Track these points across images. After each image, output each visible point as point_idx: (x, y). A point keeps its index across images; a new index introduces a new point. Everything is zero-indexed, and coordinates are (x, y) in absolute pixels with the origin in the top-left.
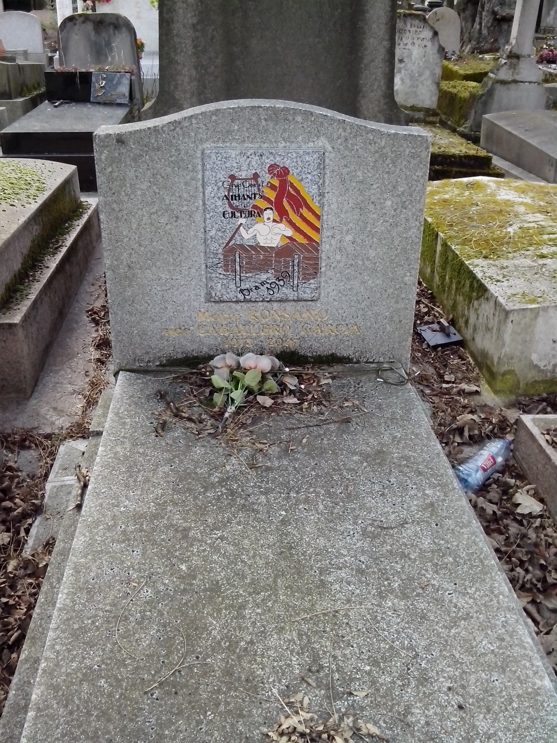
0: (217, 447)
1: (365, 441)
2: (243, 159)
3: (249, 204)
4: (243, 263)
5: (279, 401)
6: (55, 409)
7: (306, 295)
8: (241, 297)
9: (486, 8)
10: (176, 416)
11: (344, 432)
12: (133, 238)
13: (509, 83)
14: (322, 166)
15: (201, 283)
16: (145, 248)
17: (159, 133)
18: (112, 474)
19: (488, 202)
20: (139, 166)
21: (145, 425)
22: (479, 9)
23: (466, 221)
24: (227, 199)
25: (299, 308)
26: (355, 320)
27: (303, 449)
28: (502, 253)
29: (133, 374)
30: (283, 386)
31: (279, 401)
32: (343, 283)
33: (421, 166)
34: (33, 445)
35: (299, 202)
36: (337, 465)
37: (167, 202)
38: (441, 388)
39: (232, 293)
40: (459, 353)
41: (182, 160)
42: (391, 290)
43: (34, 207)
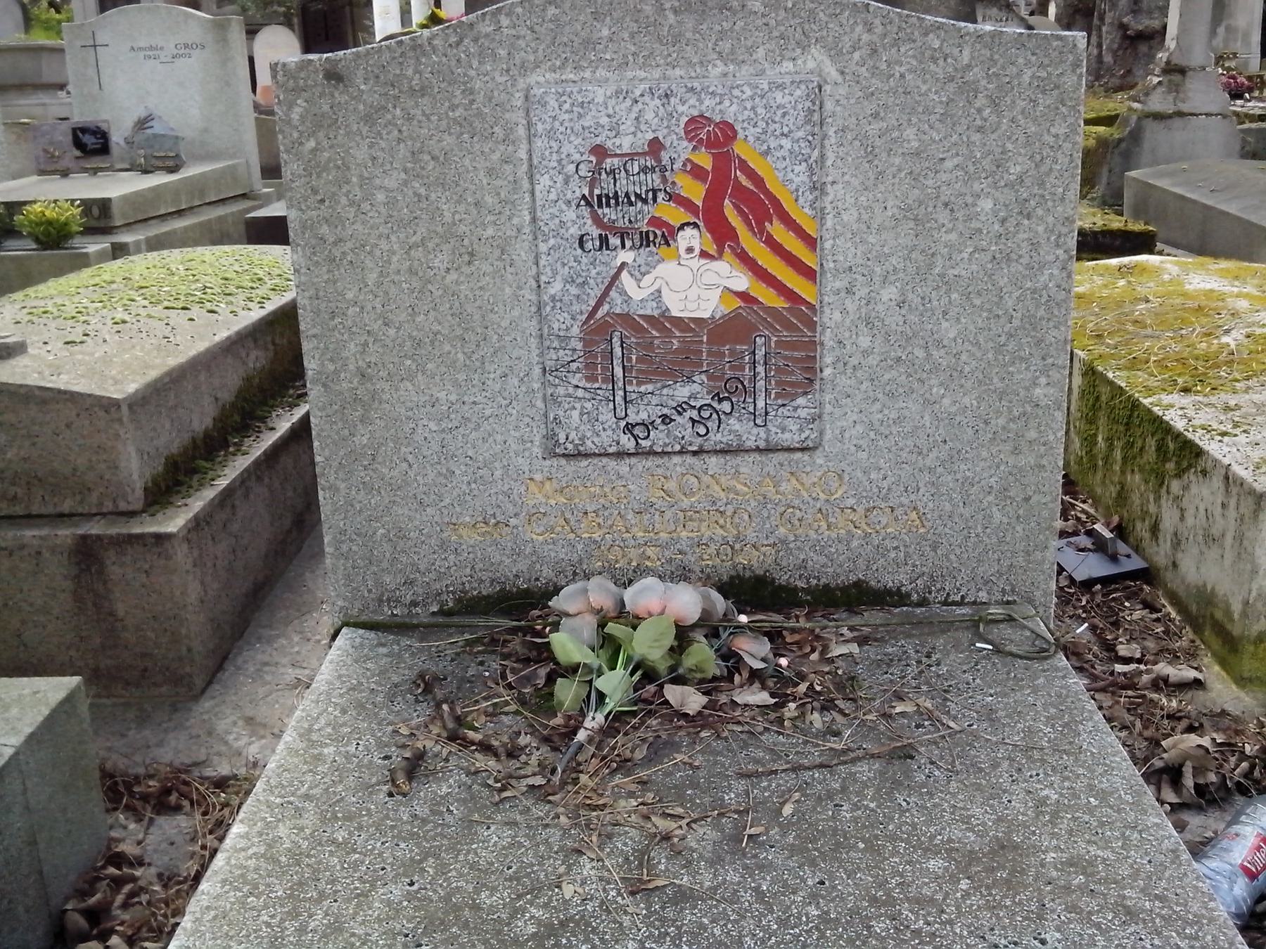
0: (547, 826)
1: (959, 813)
2: (623, 106)
3: (641, 215)
4: (630, 360)
5: (723, 699)
6: (250, 721)
7: (787, 435)
8: (628, 443)
9: (1109, 18)
10: (453, 737)
11: (897, 784)
12: (369, 307)
13: (1170, 117)
14: (816, 117)
15: (532, 412)
16: (399, 329)
17: (424, 53)
18: (243, 904)
19: (1169, 295)
20: (379, 133)
21: (371, 762)
22: (1096, 21)
23: (1130, 327)
24: (589, 204)
25: (770, 469)
26: (913, 497)
27: (784, 835)
28: (1221, 382)
29: (372, 635)
30: (731, 658)
31: (723, 699)
32: (878, 406)
33: (1064, 109)
34: (186, 803)
35: (763, 207)
36: (882, 884)
37: (448, 217)
38: (1112, 673)
39: (608, 435)
40: (1142, 596)
41: (479, 114)
42: (1001, 422)
43: (256, 314)
